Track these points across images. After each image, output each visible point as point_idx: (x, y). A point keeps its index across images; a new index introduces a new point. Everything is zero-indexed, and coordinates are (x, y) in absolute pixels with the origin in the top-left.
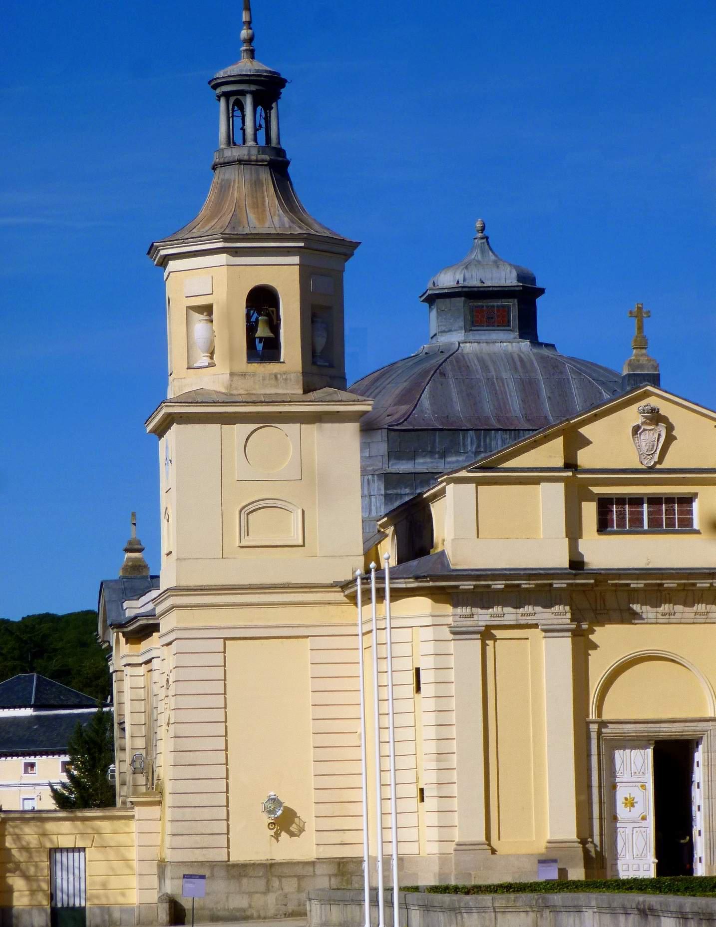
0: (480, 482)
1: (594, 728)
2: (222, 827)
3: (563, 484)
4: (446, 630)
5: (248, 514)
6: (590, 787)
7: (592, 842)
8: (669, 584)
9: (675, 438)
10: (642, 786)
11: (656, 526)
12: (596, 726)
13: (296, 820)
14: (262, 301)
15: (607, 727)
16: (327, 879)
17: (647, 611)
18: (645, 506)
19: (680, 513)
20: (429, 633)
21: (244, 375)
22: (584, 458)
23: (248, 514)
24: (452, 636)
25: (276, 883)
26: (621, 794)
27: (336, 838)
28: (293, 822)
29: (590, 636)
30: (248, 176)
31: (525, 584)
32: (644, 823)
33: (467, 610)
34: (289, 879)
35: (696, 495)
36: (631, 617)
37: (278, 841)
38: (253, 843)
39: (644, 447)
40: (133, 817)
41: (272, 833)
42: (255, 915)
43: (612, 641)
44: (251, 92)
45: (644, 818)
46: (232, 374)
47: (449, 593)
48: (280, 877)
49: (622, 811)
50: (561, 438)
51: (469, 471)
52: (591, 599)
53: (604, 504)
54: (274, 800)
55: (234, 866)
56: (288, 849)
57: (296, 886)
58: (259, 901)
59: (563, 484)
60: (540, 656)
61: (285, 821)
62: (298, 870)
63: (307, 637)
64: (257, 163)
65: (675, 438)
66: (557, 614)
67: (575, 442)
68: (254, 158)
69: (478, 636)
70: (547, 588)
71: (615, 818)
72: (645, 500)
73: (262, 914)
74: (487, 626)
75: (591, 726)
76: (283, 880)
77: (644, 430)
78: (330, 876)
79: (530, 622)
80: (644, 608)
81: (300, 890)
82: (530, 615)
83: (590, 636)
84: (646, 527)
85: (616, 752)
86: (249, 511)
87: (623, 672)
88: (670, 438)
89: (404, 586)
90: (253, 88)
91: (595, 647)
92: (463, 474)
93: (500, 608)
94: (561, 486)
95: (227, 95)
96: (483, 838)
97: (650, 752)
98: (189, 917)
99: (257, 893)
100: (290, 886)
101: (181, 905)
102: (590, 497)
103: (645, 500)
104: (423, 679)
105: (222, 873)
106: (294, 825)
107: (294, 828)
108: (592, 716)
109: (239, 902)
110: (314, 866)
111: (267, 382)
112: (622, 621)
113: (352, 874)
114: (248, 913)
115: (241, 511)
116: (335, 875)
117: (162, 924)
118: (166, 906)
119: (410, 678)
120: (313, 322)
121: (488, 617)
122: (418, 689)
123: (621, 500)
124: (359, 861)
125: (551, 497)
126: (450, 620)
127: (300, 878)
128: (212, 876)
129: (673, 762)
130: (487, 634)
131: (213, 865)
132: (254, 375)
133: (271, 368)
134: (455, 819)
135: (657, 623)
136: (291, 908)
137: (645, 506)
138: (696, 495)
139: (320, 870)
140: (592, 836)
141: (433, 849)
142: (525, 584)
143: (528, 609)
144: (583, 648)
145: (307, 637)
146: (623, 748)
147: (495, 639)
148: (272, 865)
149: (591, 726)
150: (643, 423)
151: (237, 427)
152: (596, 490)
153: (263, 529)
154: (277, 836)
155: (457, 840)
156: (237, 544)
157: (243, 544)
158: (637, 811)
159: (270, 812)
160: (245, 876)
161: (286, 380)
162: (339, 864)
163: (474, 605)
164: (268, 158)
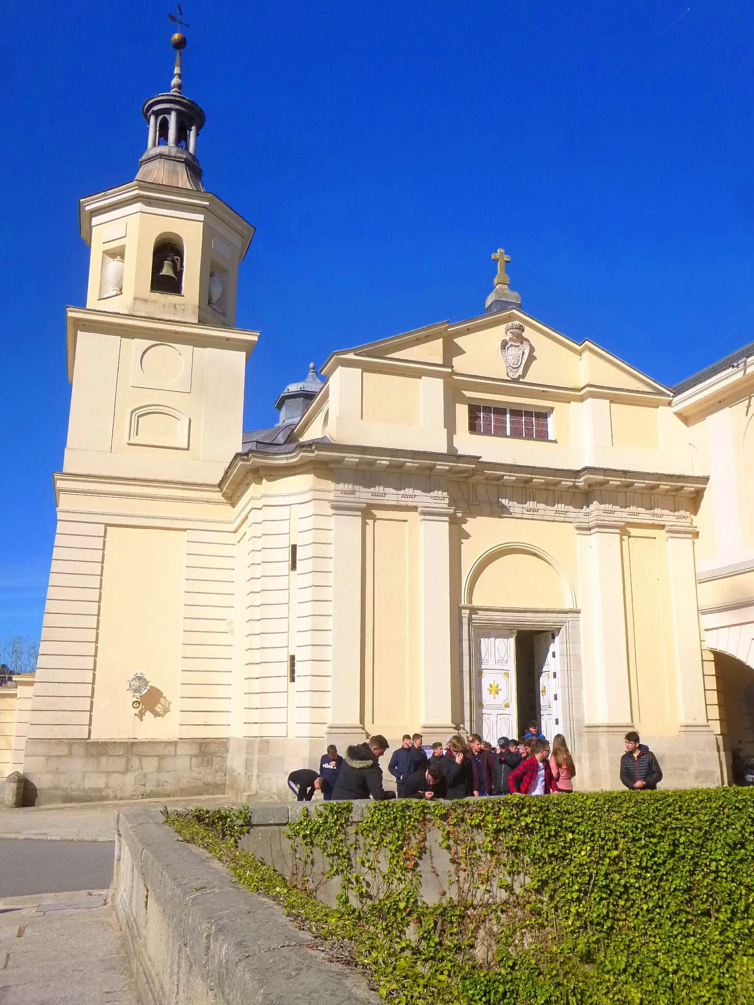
0: (367, 368)
1: (465, 613)
2: (86, 704)
3: (441, 381)
4: (327, 505)
5: (139, 417)
6: (461, 672)
7: (464, 729)
8: (538, 480)
9: (535, 358)
10: (506, 674)
11: (516, 434)
12: (468, 612)
13: (162, 700)
14: (167, 250)
15: (477, 614)
16: (188, 759)
17: (515, 507)
18: (508, 416)
19: (538, 425)
20: (309, 509)
21: (146, 301)
22: (459, 364)
23: (139, 417)
24: (334, 511)
25: (135, 762)
26: (487, 680)
27: (200, 718)
28: (159, 702)
29: (463, 526)
30: (167, 166)
31: (410, 463)
32: (506, 711)
33: (349, 487)
34: (149, 758)
35: (552, 409)
36: (501, 512)
37: (142, 720)
38: (116, 721)
39: (511, 360)
40: (15, 696)
41: (137, 711)
42: (112, 795)
43: (485, 533)
44: (176, 110)
45: (507, 706)
46: (135, 299)
47: (331, 470)
48: (141, 756)
49: (487, 698)
50: (441, 340)
51: (356, 354)
52: (473, 490)
53: (474, 410)
54: (140, 678)
55: (94, 743)
56: (151, 729)
57: (156, 765)
58: (116, 780)
59: (441, 381)
60: (417, 538)
61: (149, 700)
62: (160, 750)
63: (185, 530)
64: (175, 159)
65: (535, 358)
66: (435, 498)
67: (451, 351)
68: (173, 154)
69: (359, 513)
70: (427, 472)
71: (480, 705)
72: (508, 411)
73: (119, 794)
74: (368, 504)
75: (463, 611)
76: (144, 759)
77: (511, 346)
78: (191, 756)
79: (410, 504)
80: (511, 503)
81: (159, 769)
82: (411, 496)
83: (463, 526)
84: (508, 433)
85: (482, 639)
86: (140, 413)
87: (640, 473)
88: (531, 358)
89: (285, 462)
90: (177, 107)
91: (467, 536)
92: (351, 356)
93: (381, 488)
94: (440, 382)
95: (157, 114)
96: (357, 722)
97: (512, 642)
98: (40, 797)
99: (115, 772)
100: (150, 765)
101: (32, 784)
102: (463, 400)
103: (508, 411)
104: (299, 556)
105: (79, 750)
106: (159, 705)
107: (159, 708)
108: (464, 602)
109: (94, 782)
110: (176, 746)
111: (166, 309)
112: (492, 515)
113: (213, 754)
114: (104, 794)
115: (132, 412)
116: (196, 756)
117: (6, 806)
118: (14, 786)
119: (286, 555)
120: (211, 275)
121: (369, 496)
122: (294, 567)
123: (487, 410)
124: (223, 743)
125: (432, 390)
126: (331, 496)
127: (161, 757)
128: (70, 755)
129: (531, 647)
130: (367, 512)
131: (71, 742)
132: (156, 302)
133: (173, 298)
134: (328, 699)
135: (522, 518)
136: (148, 788)
137: (508, 416)
138: (552, 409)
139: (182, 750)
140: (463, 722)
141: (306, 731)
142: (410, 463)
143: (409, 491)
144: (457, 536)
145: (185, 530)
146: (488, 636)
147: (375, 519)
148: (133, 744)
149: (463, 611)
150: (511, 339)
151: (137, 341)
152: (468, 394)
153: (152, 429)
154: (141, 715)
155: (330, 722)
156: (126, 441)
157: (132, 441)
158: (501, 699)
159: (136, 691)
160: (104, 755)
161: (184, 310)
162: (201, 744)
163: (355, 483)
164: (185, 156)
